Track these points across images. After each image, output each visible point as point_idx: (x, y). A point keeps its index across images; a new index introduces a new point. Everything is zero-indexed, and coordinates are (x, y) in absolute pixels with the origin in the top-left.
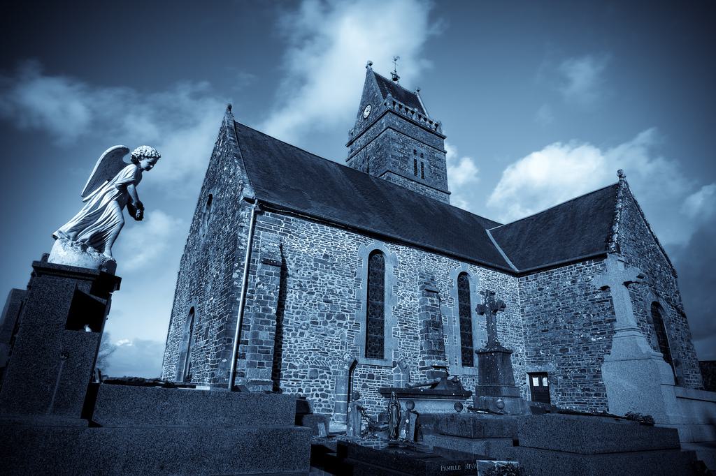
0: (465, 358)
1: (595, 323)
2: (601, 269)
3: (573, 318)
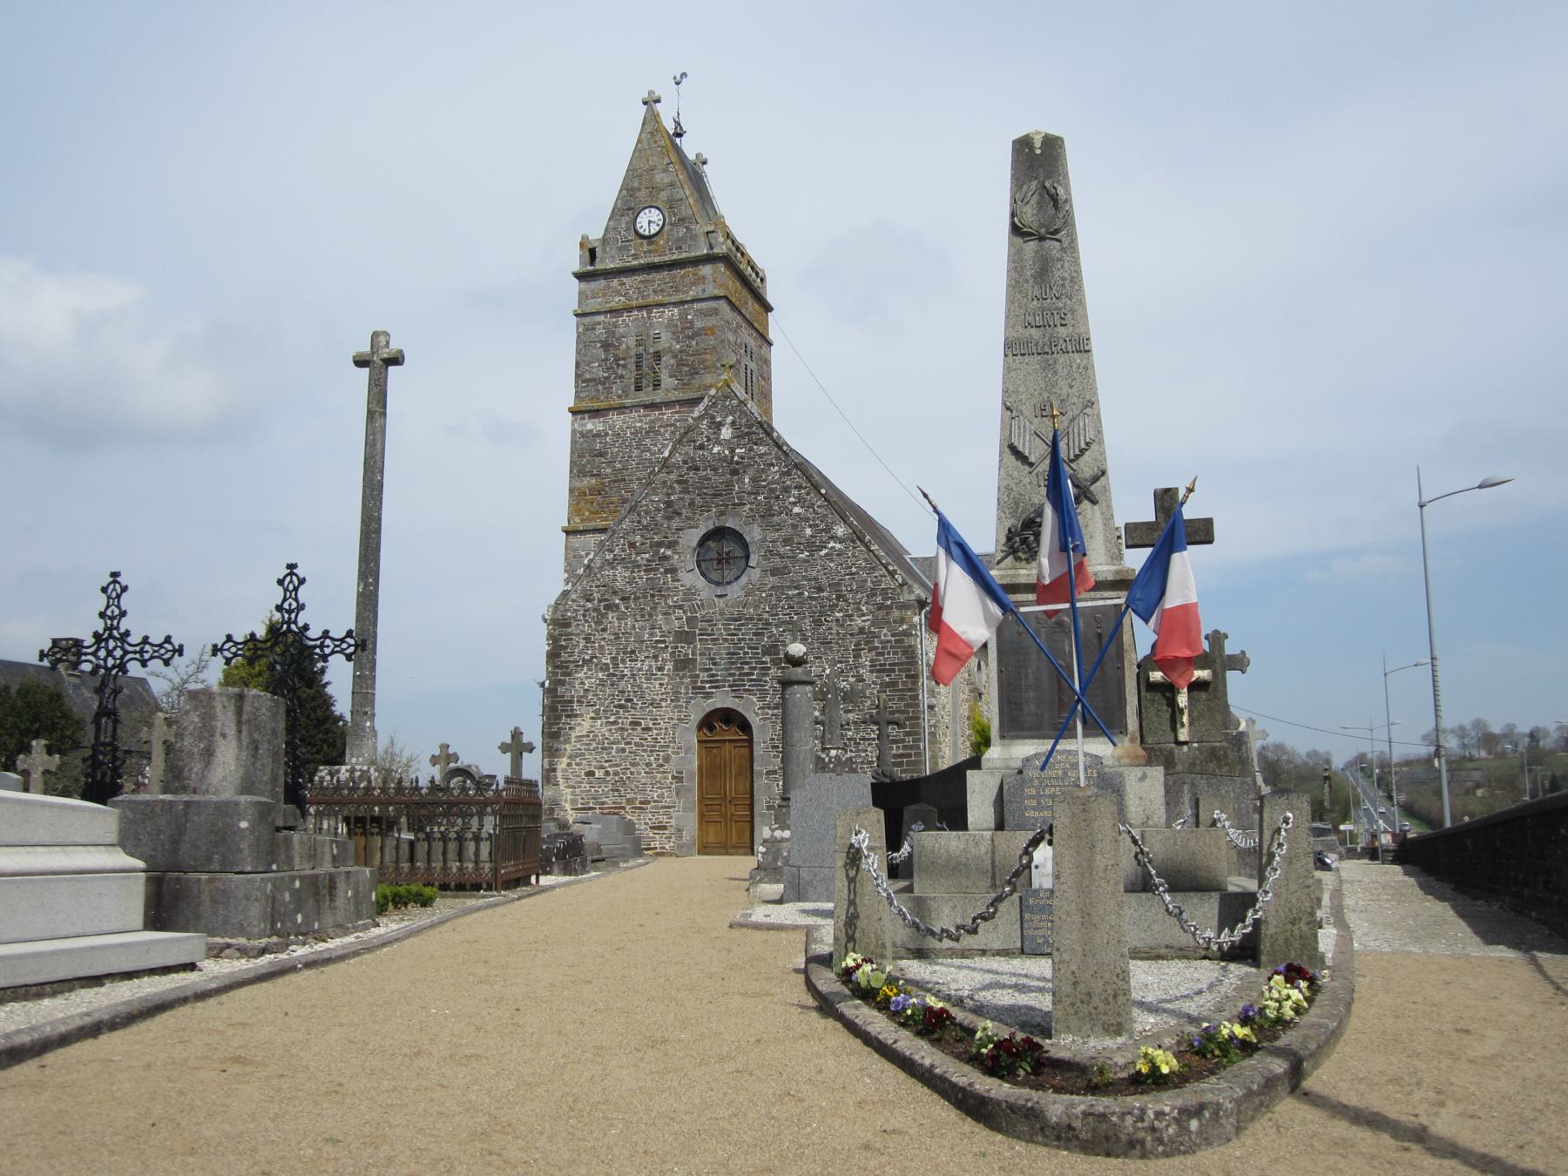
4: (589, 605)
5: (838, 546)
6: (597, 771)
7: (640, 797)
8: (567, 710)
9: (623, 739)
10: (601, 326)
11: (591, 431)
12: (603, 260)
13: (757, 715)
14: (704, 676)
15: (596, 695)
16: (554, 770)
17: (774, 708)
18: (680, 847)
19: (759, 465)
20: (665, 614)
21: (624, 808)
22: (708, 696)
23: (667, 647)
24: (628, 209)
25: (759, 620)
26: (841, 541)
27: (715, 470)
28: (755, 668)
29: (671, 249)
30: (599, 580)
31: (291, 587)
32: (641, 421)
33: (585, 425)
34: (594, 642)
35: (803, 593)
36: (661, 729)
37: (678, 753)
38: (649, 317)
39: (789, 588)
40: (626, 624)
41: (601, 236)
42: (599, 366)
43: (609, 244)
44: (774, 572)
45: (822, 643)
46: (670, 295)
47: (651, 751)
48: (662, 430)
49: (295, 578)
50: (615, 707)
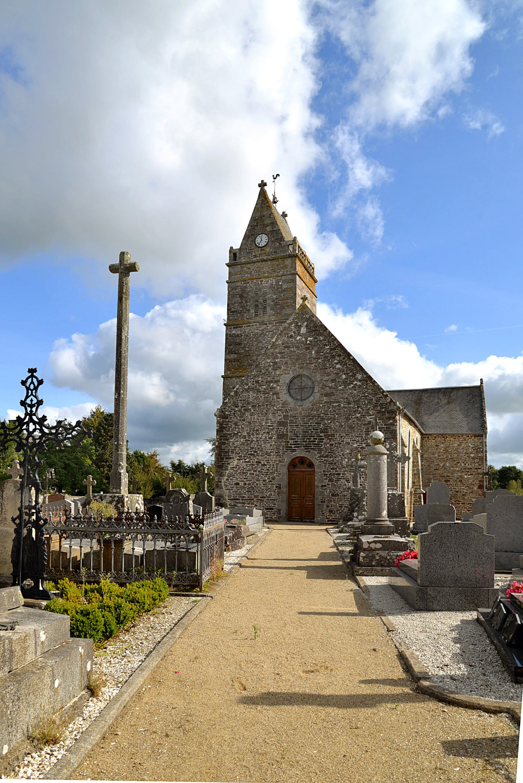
0: (176, 779)
1: (468, 469)
2: (477, 441)
3: (456, 464)
4: (237, 409)
5: (358, 383)
6: (240, 483)
7: (260, 495)
8: (226, 456)
9: (253, 469)
10: (239, 288)
11: (235, 334)
12: (240, 258)
13: (317, 460)
14: (291, 442)
15: (240, 449)
16: (220, 482)
17: (325, 457)
18: (279, 518)
19: (320, 345)
20: (273, 413)
21: (253, 499)
22: (294, 451)
23: (274, 428)
24: (252, 235)
25: (318, 417)
26: (360, 381)
27: (298, 347)
28: (316, 439)
29: (272, 253)
30: (241, 397)
31: (32, 387)
32: (257, 329)
33: (232, 331)
34: (239, 426)
35: (340, 405)
36: (271, 465)
37: (278, 476)
38: (261, 283)
39: (334, 402)
40: (254, 418)
41: (239, 247)
42: (238, 305)
43: (242, 251)
44: (326, 395)
45: (349, 428)
46: (271, 273)
47: (266, 475)
48: (267, 334)
49: (35, 380)
50: (249, 455)
